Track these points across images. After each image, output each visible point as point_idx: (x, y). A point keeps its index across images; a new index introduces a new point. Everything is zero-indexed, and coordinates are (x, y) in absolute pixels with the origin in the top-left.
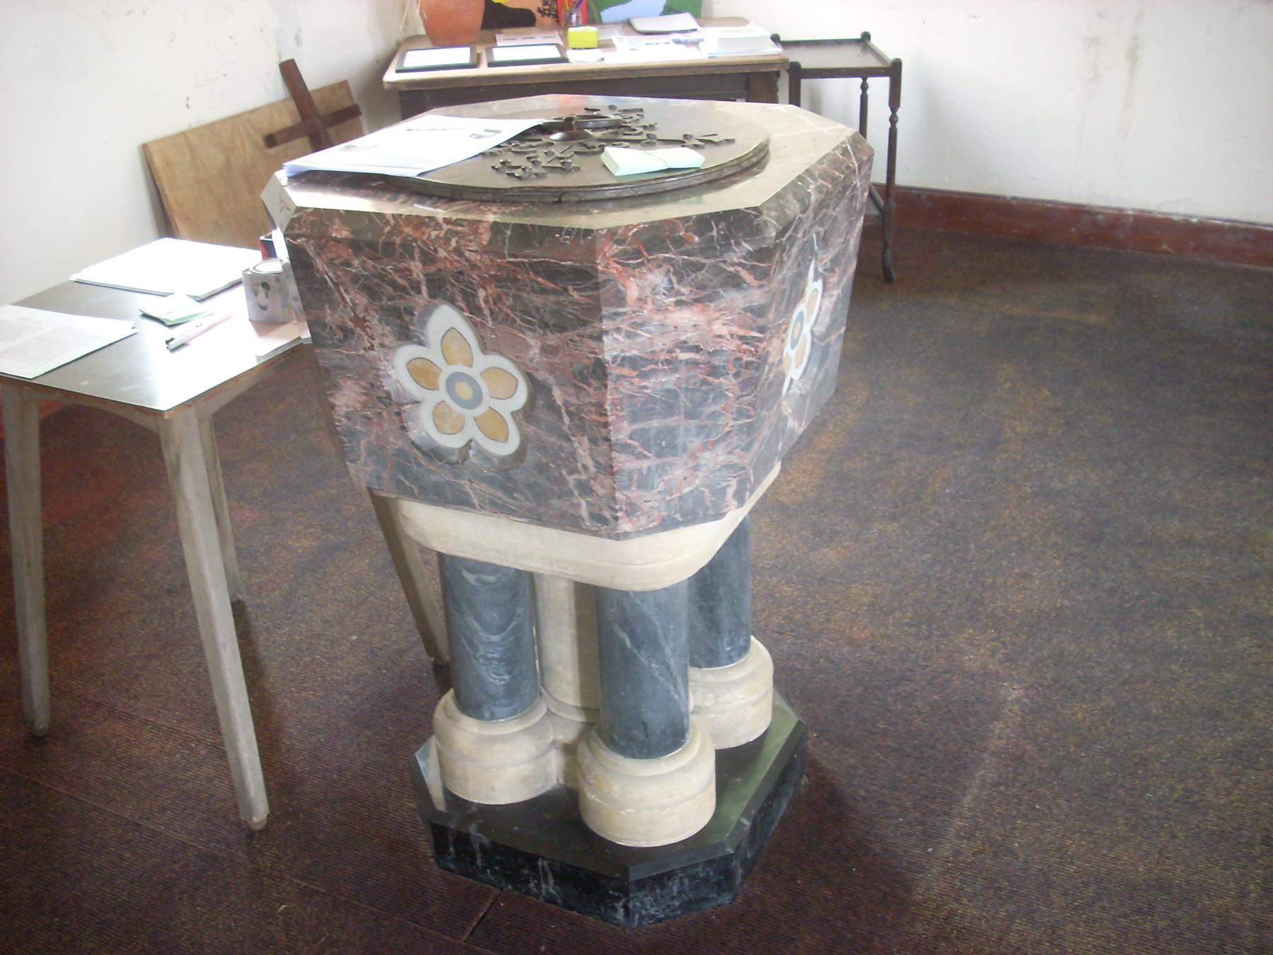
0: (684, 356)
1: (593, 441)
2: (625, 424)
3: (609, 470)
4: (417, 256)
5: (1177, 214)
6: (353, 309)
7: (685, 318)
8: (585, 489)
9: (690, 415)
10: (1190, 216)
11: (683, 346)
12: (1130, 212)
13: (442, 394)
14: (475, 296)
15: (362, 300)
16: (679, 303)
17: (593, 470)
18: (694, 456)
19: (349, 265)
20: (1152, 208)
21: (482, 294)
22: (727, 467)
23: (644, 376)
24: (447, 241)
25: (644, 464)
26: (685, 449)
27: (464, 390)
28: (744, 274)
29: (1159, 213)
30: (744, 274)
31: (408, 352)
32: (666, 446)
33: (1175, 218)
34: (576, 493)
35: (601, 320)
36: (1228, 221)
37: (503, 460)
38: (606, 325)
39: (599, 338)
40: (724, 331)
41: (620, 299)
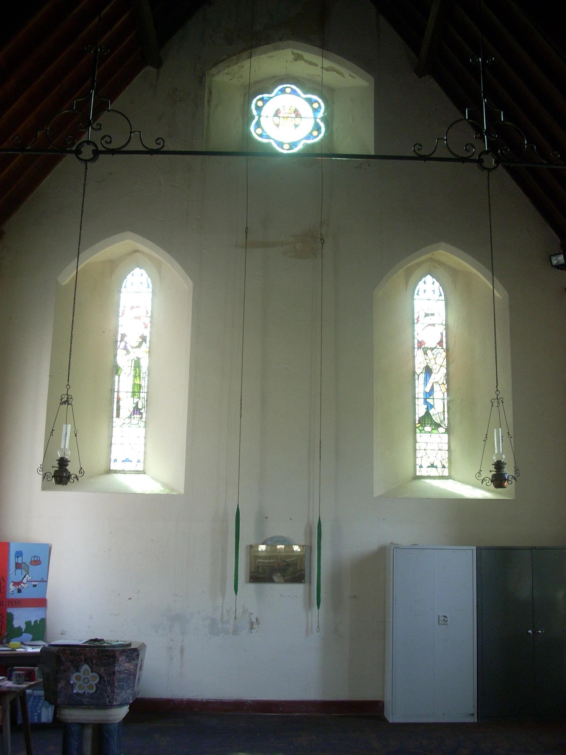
0: (126, 671)
1: (111, 686)
2: (117, 683)
3: (113, 692)
4: (83, 655)
5: (199, 699)
6: (68, 666)
7: (127, 665)
8: (108, 696)
9: (126, 683)
10: (203, 699)
11: (126, 670)
12: (185, 700)
13: (81, 682)
14: (93, 662)
15: (70, 664)
16: (126, 662)
17: (110, 692)
18: (126, 691)
19: (69, 658)
20: (191, 698)
21: (94, 661)
22: (131, 693)
23: (120, 674)
24: (89, 652)
25: (119, 691)
26: (125, 689)
27: (86, 681)
28: (135, 658)
29: (193, 699)
30: (135, 658)
31: (76, 674)
32: (122, 688)
33: (199, 700)
34: (106, 697)
35: (115, 664)
36: (214, 699)
37: (92, 694)
38: (116, 665)
39: (115, 667)
40: (132, 668)
41: (118, 661)
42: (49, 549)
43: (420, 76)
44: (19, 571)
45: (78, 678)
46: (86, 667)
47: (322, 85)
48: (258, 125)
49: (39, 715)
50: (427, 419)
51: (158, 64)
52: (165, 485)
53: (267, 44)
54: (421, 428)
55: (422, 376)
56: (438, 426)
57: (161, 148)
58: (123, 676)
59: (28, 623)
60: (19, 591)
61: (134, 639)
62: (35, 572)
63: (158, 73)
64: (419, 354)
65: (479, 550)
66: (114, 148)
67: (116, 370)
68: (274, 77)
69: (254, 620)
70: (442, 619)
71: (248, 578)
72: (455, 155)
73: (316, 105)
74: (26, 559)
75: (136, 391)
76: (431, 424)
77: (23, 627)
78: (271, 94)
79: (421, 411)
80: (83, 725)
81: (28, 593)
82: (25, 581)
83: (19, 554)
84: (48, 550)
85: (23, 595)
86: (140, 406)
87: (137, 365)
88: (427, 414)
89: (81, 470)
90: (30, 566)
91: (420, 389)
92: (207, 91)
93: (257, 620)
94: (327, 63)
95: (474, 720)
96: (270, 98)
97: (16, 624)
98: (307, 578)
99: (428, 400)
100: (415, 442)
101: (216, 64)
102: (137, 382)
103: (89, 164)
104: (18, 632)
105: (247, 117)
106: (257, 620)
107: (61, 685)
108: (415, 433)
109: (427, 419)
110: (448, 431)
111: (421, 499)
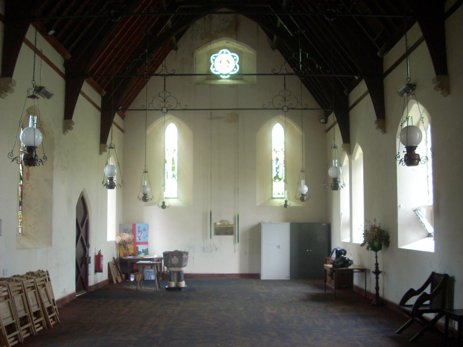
31: (173, 259)
43: (273, 49)
44: (139, 233)
45: (173, 260)
46: (175, 257)
47: (237, 50)
48: (214, 67)
49: (151, 277)
50: (277, 177)
51: (176, 49)
53: (216, 39)
54: (275, 180)
55: (275, 162)
57: (187, 108)
58: (185, 259)
59: (143, 250)
60: (140, 239)
62: (144, 233)
63: (176, 52)
64: (274, 153)
66: (173, 108)
67: (165, 162)
68: (219, 47)
69: (217, 248)
70: (278, 246)
72: (275, 107)
73: (235, 58)
74: (141, 229)
76: (278, 179)
77: (142, 251)
79: (274, 174)
80: (174, 272)
81: (142, 240)
82: (141, 236)
85: (141, 241)
86: (175, 175)
87: (173, 160)
88: (277, 175)
89: (153, 197)
91: (274, 166)
92: (195, 59)
94: (238, 45)
95: (289, 279)
96: (218, 56)
98: (234, 233)
99: (277, 170)
100: (272, 185)
101: (198, 48)
102: (173, 166)
103: (165, 114)
104: (140, 253)
105: (209, 64)
106: (218, 247)
107: (169, 261)
108: (272, 182)
109: (277, 177)
110: (285, 181)
111: (275, 207)
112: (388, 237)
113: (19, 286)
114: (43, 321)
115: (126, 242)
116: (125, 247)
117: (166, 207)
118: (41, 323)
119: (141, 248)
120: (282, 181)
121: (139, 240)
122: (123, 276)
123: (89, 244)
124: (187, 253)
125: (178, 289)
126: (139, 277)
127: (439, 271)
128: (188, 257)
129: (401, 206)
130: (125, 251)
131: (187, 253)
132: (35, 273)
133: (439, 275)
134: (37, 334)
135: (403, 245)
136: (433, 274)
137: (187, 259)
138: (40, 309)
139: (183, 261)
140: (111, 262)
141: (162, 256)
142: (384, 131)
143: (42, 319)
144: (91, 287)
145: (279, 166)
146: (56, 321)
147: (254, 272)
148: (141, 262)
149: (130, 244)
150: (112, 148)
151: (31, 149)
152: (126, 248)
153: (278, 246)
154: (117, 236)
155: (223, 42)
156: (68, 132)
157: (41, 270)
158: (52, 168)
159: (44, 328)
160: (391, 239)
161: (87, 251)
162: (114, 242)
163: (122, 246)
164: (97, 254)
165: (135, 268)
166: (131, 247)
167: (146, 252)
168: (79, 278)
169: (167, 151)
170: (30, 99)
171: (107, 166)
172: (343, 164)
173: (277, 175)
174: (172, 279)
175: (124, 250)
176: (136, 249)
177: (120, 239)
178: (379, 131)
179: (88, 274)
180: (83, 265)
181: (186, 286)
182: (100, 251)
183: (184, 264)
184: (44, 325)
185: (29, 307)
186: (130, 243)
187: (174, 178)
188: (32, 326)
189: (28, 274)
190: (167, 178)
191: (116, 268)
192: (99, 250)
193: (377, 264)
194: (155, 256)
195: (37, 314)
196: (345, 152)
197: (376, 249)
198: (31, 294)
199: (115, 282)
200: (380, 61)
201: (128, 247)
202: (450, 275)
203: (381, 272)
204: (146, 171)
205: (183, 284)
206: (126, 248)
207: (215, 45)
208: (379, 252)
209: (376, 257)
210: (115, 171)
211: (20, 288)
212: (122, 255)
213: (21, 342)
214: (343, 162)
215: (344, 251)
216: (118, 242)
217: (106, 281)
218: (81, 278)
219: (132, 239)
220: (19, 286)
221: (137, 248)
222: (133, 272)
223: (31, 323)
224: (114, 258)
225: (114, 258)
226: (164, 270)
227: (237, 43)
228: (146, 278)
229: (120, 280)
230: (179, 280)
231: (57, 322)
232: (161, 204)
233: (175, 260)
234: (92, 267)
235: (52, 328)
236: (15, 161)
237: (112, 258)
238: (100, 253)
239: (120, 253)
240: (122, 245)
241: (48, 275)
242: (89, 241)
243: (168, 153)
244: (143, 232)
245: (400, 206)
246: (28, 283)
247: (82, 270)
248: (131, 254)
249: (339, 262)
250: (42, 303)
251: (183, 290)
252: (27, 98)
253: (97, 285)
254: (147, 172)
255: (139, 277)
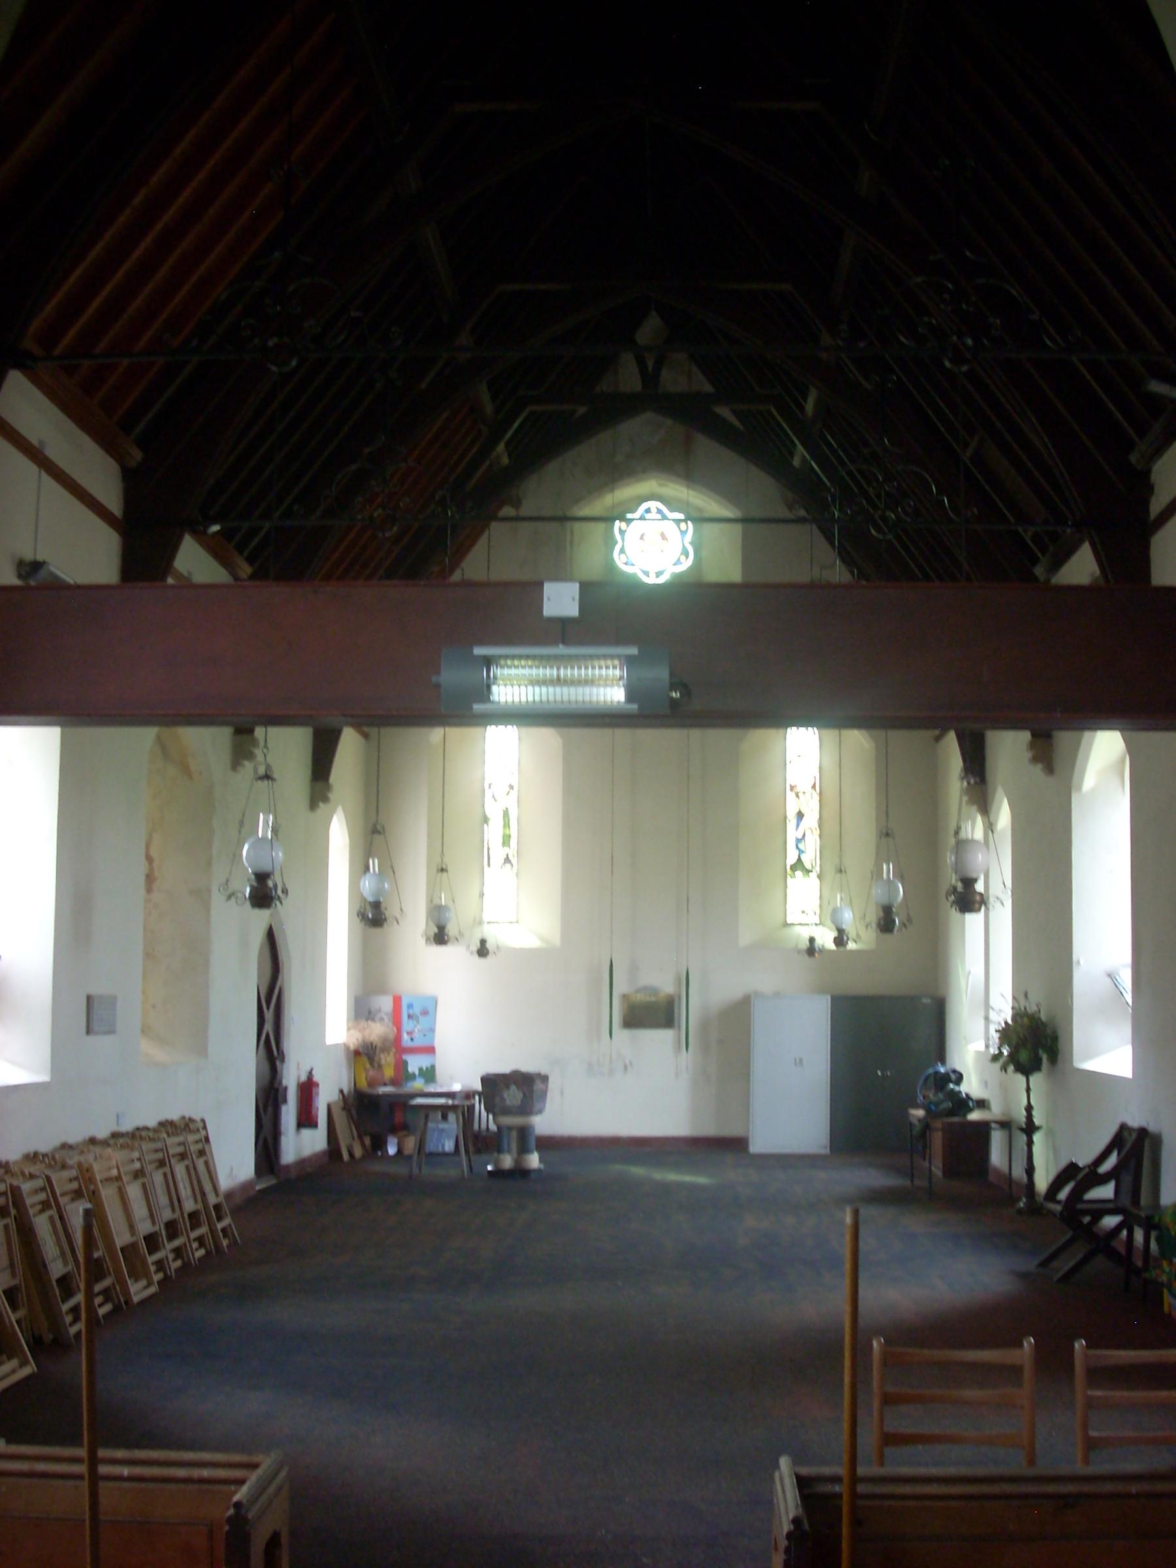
42: (435, 1001)
44: (411, 1022)
46: (513, 1088)
48: (622, 551)
49: (443, 1146)
50: (799, 865)
52: (542, 938)
56: (808, 871)
59: (421, 1070)
60: (412, 1039)
61: (544, 1070)
64: (790, 796)
65: (834, 999)
69: (628, 1064)
71: (622, 1024)
74: (417, 1010)
75: (506, 840)
77: (417, 1073)
78: (634, 512)
79: (791, 859)
80: (510, 1128)
81: (419, 1041)
83: (410, 1006)
84: (613, 1036)
87: (506, 814)
88: (799, 859)
90: (420, 1017)
91: (792, 834)
93: (631, 1063)
94: (691, 492)
97: (410, 1069)
102: (507, 832)
104: (413, 1077)
106: (631, 1063)
109: (799, 865)
112: (1055, 1038)
113: (156, 1151)
114: (206, 1236)
115: (376, 1047)
116: (371, 1059)
117: (490, 955)
118: (201, 1240)
119: (414, 1064)
120: (813, 875)
121: (409, 1040)
122: (367, 1141)
123: (283, 1053)
124: (545, 1079)
125: (521, 1173)
126: (411, 1143)
127: (1134, 1122)
128: (547, 1087)
129: (1082, 962)
130: (371, 1073)
131: (545, 1079)
132: (178, 1125)
133: (1130, 1130)
134: (197, 1262)
135: (1089, 1057)
136: (1123, 1127)
137: (544, 1093)
138: (200, 1206)
139: (535, 1098)
140: (335, 1103)
141: (478, 1087)
142: (1050, 769)
143: (203, 1230)
144: (287, 1167)
145: (804, 835)
146: (229, 1239)
147: (731, 1130)
148: (420, 1101)
149: (386, 1053)
150: (379, 833)
151: (262, 877)
152: (376, 1065)
153: (798, 1060)
154: (349, 1029)
155: (650, 485)
156: (243, 766)
157: (187, 1116)
158: (209, 864)
159: (208, 1253)
160: (1062, 1045)
161: (278, 1070)
162: (343, 1045)
163: (365, 1059)
164: (304, 1078)
165: (398, 1117)
166: (388, 1060)
167: (429, 1074)
168: (261, 1142)
169: (490, 787)
170: (260, 782)
171: (368, 875)
172: (996, 824)
173: (799, 859)
174: (506, 1147)
175: (366, 1071)
176: (401, 1066)
177: (360, 1039)
178: (1038, 769)
179: (280, 1134)
180: (270, 1109)
181: (542, 1166)
182: (310, 1073)
183: (537, 1106)
184: (208, 1246)
185: (179, 1201)
186: (385, 1049)
187: (508, 865)
188: (188, 1243)
189: (162, 1124)
190: (489, 865)
191: (348, 1119)
192: (308, 1069)
193: (1029, 1108)
194: (457, 1087)
195: (194, 1216)
196: (974, 808)
197: (1027, 1069)
198: (180, 1169)
199: (346, 1156)
200: (1142, 485)
201: (380, 1059)
202: (1152, 1128)
203: (1038, 1128)
204: (444, 867)
205: (534, 1160)
206: (376, 1065)
207: (626, 492)
208: (1036, 1079)
209: (1028, 1090)
210: (386, 886)
211: (160, 1155)
212: (363, 1084)
213: (171, 1276)
214: (997, 819)
215: (958, 1075)
216: (352, 1047)
217: (324, 1153)
218: (265, 1140)
219: (392, 1037)
220: (156, 1151)
221: (406, 1063)
222: (394, 1130)
223: (185, 1236)
224: (341, 1091)
225: (341, 1091)
226: (480, 1127)
227: (688, 487)
228: (431, 1147)
229: (358, 1152)
230: (524, 1149)
231: (232, 1241)
232: (476, 945)
233: (512, 1096)
234: (289, 1113)
235: (225, 1252)
236: (233, 899)
237: (338, 1091)
238: (310, 1074)
239: (357, 1080)
240: (363, 1055)
241: (205, 1127)
242: (283, 1043)
243: (493, 796)
244: (422, 1019)
245: (1078, 962)
246: (173, 1143)
247: (266, 1121)
248: (387, 1082)
249: (942, 1101)
250: (203, 1194)
251: (533, 1175)
252: (254, 781)
253: (302, 1163)
254: (447, 871)
255: (411, 1143)
